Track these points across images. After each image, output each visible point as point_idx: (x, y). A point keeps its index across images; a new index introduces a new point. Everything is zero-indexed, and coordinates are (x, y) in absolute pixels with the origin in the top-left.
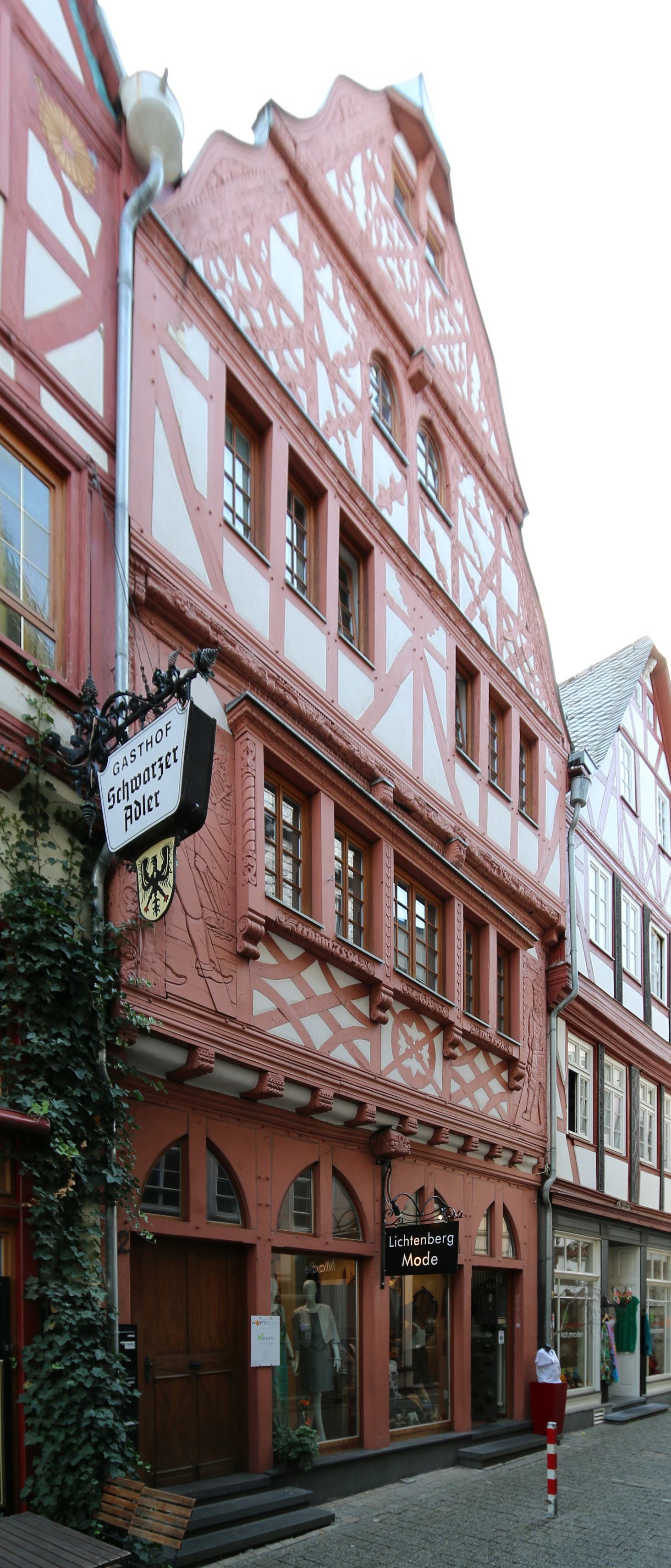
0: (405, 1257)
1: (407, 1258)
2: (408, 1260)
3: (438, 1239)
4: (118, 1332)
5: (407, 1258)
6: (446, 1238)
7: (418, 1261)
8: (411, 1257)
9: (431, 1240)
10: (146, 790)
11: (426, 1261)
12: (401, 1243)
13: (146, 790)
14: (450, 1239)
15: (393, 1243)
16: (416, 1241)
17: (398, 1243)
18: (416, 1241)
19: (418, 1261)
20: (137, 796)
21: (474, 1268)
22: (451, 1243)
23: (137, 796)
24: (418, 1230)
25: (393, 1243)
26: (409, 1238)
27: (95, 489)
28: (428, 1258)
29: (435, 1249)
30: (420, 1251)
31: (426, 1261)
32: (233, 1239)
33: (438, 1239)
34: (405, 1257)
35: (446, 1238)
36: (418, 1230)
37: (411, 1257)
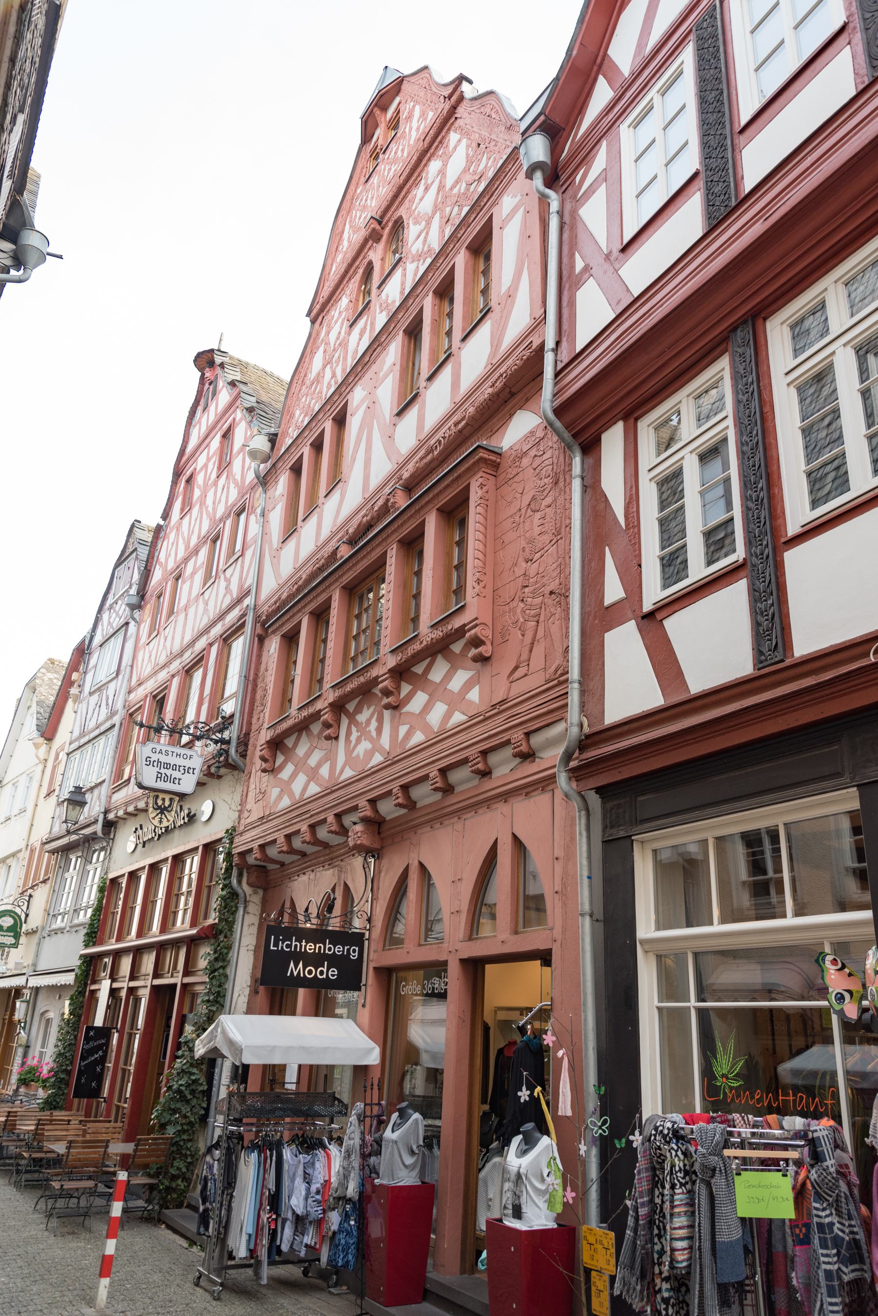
0: (292, 965)
1: (296, 967)
2: (295, 969)
3: (338, 949)
4: (790, 921)
5: (296, 967)
6: (348, 950)
7: (310, 972)
8: (301, 965)
9: (330, 949)
10: (176, 774)
11: (322, 973)
12: (288, 946)
13: (176, 774)
14: (354, 951)
15: (276, 945)
16: (310, 948)
17: (283, 946)
18: (310, 948)
19: (310, 972)
20: (169, 772)
21: (462, 961)
22: (354, 956)
23: (169, 772)
24: (318, 935)
25: (276, 945)
26: (301, 942)
27: (853, 1198)
28: (325, 970)
29: (333, 961)
30: (316, 960)
31: (322, 973)
32: (514, 951)
33: (338, 949)
34: (292, 965)
35: (348, 950)
36: (318, 935)
37: (301, 965)
